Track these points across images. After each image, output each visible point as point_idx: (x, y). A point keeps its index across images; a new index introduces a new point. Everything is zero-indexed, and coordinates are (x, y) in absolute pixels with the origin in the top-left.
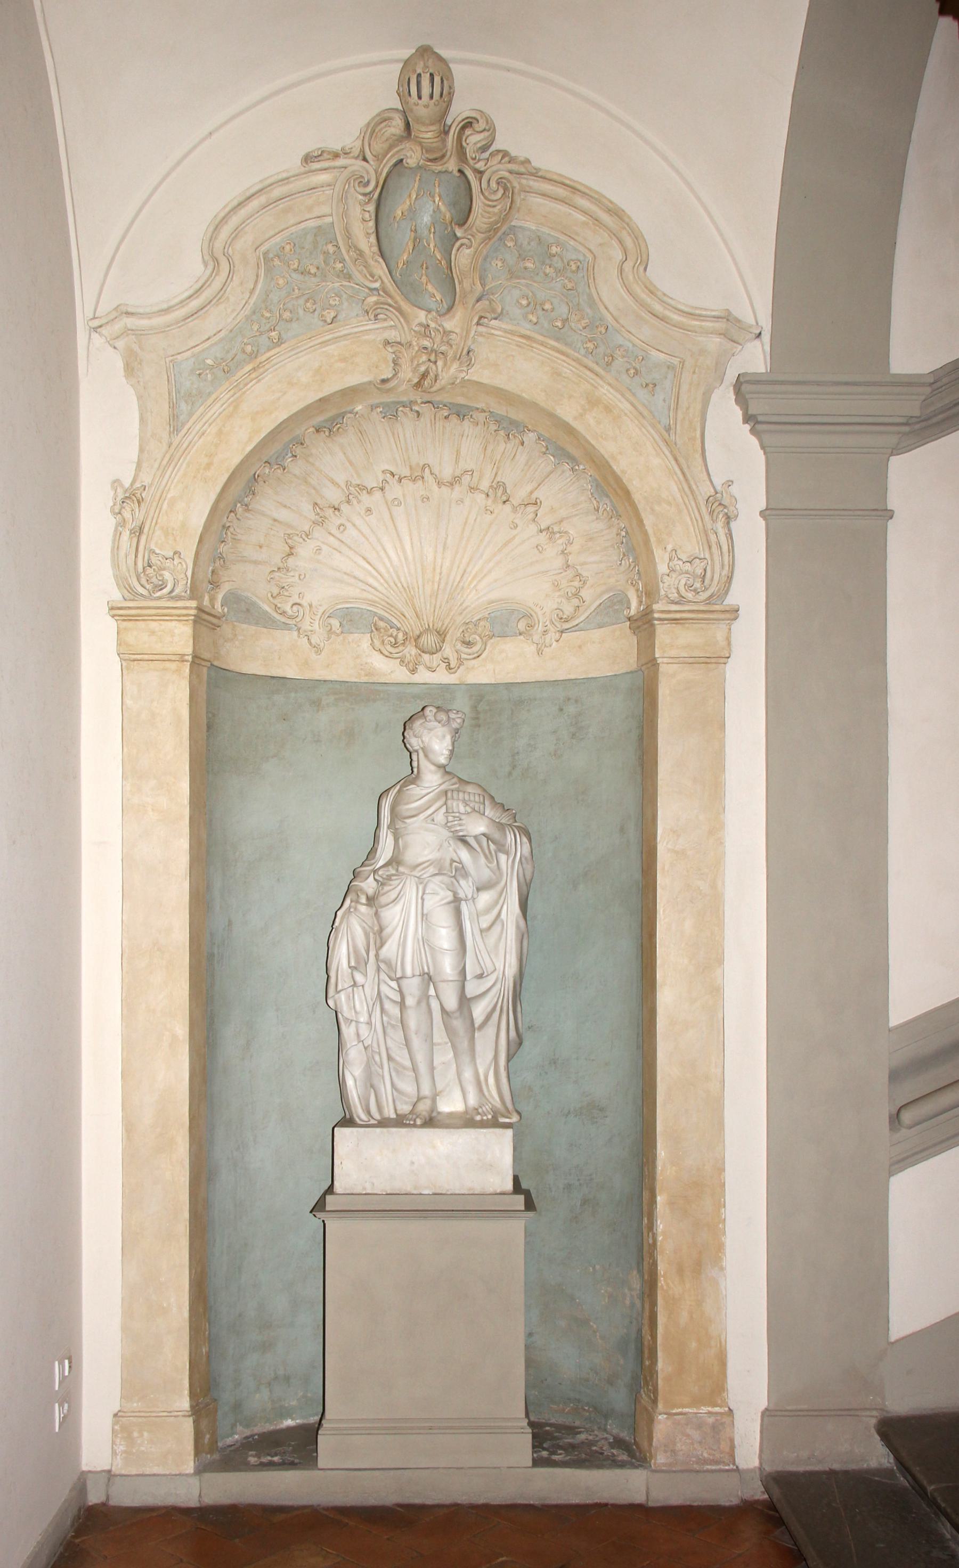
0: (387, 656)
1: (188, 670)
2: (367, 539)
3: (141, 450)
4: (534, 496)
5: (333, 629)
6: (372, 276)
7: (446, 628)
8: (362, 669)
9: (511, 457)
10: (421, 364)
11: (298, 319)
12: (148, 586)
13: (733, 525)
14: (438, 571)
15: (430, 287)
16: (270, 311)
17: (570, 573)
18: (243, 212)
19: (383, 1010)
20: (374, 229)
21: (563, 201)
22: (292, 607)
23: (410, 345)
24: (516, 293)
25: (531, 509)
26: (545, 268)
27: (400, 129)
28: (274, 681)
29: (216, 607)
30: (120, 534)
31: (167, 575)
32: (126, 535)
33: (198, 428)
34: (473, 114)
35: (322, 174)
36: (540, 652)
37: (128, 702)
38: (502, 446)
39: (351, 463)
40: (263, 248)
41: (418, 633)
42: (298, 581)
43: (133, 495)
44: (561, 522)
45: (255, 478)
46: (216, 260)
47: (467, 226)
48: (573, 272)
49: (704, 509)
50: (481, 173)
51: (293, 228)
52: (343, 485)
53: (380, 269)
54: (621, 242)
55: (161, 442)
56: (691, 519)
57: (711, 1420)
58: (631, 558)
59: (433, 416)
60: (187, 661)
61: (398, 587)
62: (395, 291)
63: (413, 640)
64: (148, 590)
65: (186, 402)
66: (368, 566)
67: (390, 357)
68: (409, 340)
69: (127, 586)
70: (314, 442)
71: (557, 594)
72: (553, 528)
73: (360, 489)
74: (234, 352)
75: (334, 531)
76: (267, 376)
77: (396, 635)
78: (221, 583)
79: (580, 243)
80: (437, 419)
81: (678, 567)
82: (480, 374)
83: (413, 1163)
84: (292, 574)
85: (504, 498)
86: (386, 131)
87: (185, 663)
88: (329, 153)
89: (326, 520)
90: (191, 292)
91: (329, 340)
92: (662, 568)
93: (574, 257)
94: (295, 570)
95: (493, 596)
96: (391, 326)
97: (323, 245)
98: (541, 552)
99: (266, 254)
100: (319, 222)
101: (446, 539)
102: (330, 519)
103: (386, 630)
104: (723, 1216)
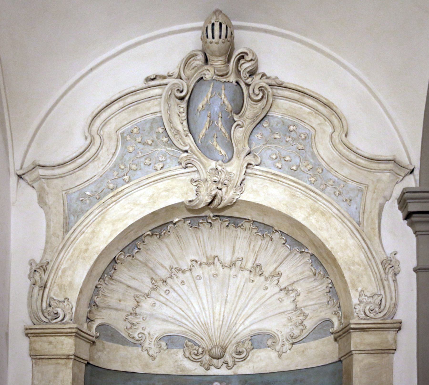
0: (192, 361)
1: (71, 364)
2: (182, 298)
3: (47, 242)
4: (277, 270)
5: (162, 346)
6: (184, 143)
7: (226, 345)
8: (178, 368)
9: (265, 248)
11: (140, 169)
12: (48, 317)
13: (398, 277)
14: (222, 314)
15: (218, 148)
16: (124, 165)
17: (299, 312)
20: (185, 118)
21: (297, 101)
24: (269, 152)
26: (287, 138)
27: (202, 62)
28: (127, 374)
30: (33, 289)
31: (60, 311)
32: (36, 289)
35: (156, 88)
36: (280, 356)
38: (260, 242)
39: (172, 255)
41: (210, 348)
42: (142, 321)
43: (41, 267)
44: (293, 283)
45: (114, 260)
48: (303, 140)
49: (380, 266)
50: (248, 85)
51: (139, 119)
52: (168, 268)
53: (190, 140)
55: (58, 238)
56: (372, 273)
58: (335, 299)
59: (220, 226)
60: (71, 359)
62: (198, 151)
63: (207, 352)
64: (48, 319)
65: (74, 215)
66: (182, 313)
68: (206, 177)
69: (36, 318)
70: (150, 241)
71: (290, 324)
72: (288, 288)
73: (178, 270)
74: (103, 187)
75: (163, 294)
76: (121, 200)
78: (95, 319)
79: (307, 124)
80: (222, 228)
81: (365, 300)
82: (247, 196)
84: (138, 317)
85: (260, 273)
86: (194, 63)
87: (70, 360)
89: (158, 288)
92: (355, 301)
93: (303, 132)
94: (140, 315)
95: (254, 327)
96: (195, 171)
97: (156, 128)
98: (281, 302)
99: (122, 134)
100: (153, 116)
101: (227, 297)
102: (160, 287)
103: (191, 346)
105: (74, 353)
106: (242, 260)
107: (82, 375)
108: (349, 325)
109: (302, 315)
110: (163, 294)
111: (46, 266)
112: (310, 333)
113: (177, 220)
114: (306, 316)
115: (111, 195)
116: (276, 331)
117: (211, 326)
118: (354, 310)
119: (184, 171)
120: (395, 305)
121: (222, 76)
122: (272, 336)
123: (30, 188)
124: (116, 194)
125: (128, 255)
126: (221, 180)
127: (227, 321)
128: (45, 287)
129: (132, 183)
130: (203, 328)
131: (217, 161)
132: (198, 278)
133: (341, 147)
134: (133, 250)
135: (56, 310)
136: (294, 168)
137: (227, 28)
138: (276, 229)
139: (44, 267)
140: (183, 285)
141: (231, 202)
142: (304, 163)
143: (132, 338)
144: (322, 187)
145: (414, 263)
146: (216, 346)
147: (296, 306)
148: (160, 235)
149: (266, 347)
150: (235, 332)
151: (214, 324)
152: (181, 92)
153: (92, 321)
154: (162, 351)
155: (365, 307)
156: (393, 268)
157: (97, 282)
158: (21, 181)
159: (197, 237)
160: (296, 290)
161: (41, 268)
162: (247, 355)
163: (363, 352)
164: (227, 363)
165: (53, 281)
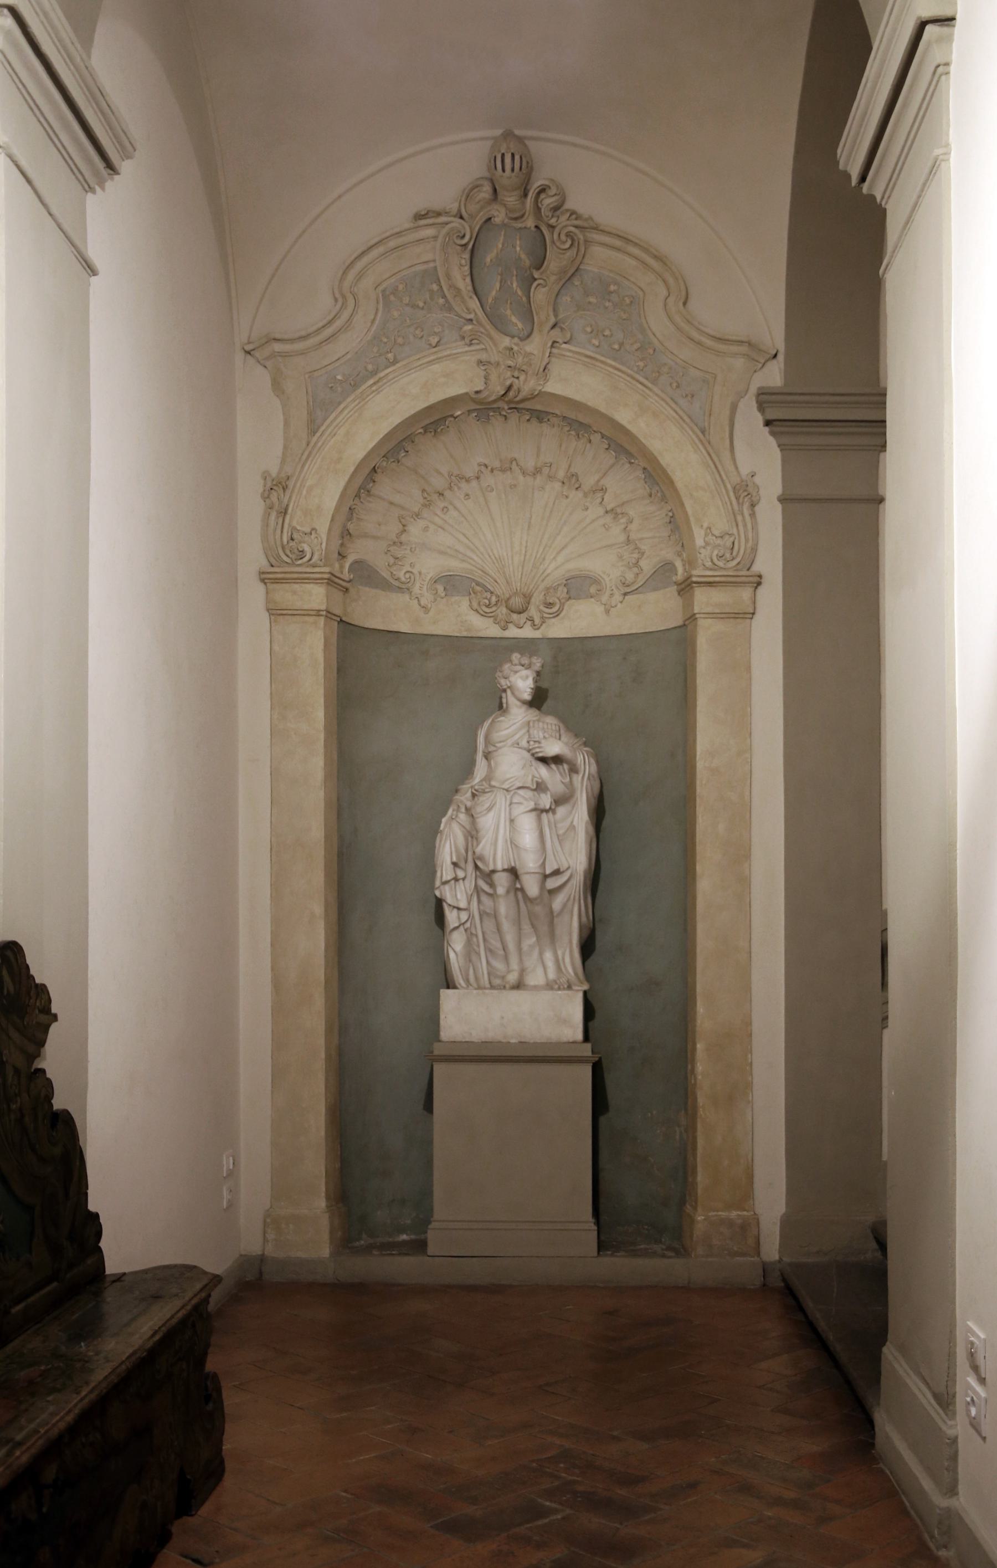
0: (482, 615)
2: (466, 519)
4: (602, 482)
5: (439, 591)
10: (507, 379)
12: (291, 556)
13: (756, 508)
15: (514, 319)
16: (388, 338)
18: (365, 260)
19: (479, 901)
20: (468, 272)
21: (618, 249)
22: (405, 573)
23: (498, 364)
25: (599, 495)
29: (344, 573)
30: (269, 515)
32: (274, 515)
33: (330, 430)
34: (547, 183)
36: (607, 612)
37: (276, 648)
40: (381, 288)
42: (410, 553)
43: (280, 483)
44: (623, 504)
45: (374, 470)
46: (344, 297)
47: (541, 270)
49: (732, 494)
50: (552, 227)
53: (474, 304)
54: (664, 281)
57: (739, 1221)
60: (322, 615)
61: (491, 559)
63: (503, 601)
64: (291, 558)
66: (467, 541)
67: (483, 373)
68: (497, 359)
73: (460, 478)
75: (439, 513)
76: (385, 388)
77: (490, 598)
81: (712, 541)
82: (553, 387)
83: (503, 1018)
84: (405, 547)
85: (577, 486)
88: (434, 212)
89: (432, 504)
90: (325, 322)
91: (434, 360)
92: (699, 542)
95: (571, 565)
96: (483, 349)
99: (384, 291)
101: (531, 518)
104: (750, 1060)
105: (327, 608)
106: (551, 466)
107: (334, 640)
108: (688, 578)
109: (637, 551)
110: (439, 513)
111: (285, 483)
112: (647, 580)
113: (459, 413)
114: (643, 554)
115: (371, 382)
116: (600, 573)
117: (508, 562)
118: (698, 555)
119: (467, 349)
120: (754, 550)
121: (516, 219)
122: (596, 581)
123: (261, 368)
124: (378, 381)
125: (392, 460)
126: (518, 365)
127: (531, 555)
128: (285, 513)
129: (398, 365)
130: (497, 565)
131: (513, 337)
132: (489, 489)
133: (678, 319)
134: (398, 453)
135: (301, 547)
136: (616, 347)
137: (521, 157)
138: (595, 429)
139: (284, 484)
140: (467, 499)
141: (532, 394)
142: (630, 340)
143: (396, 580)
144: (654, 375)
145: (777, 489)
146: (515, 593)
147: (629, 537)
148: (435, 431)
149: (587, 597)
150: (543, 573)
151: (512, 560)
152: (463, 237)
153: (344, 557)
154: (439, 599)
155: (713, 552)
156: (750, 496)
157: (351, 502)
158: (249, 356)
159: (486, 433)
160: (626, 514)
161: (280, 485)
162: (561, 609)
163: (711, 616)
164: (533, 621)
165: (296, 504)
